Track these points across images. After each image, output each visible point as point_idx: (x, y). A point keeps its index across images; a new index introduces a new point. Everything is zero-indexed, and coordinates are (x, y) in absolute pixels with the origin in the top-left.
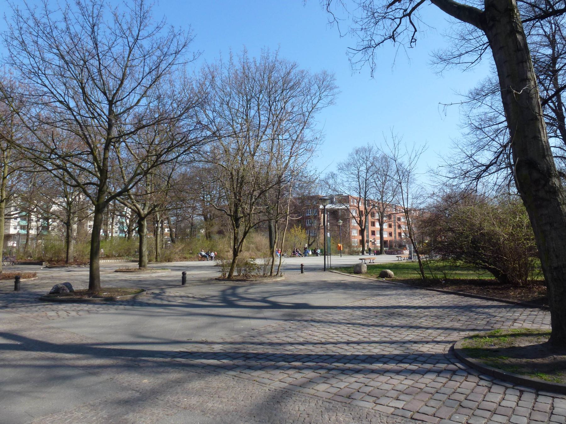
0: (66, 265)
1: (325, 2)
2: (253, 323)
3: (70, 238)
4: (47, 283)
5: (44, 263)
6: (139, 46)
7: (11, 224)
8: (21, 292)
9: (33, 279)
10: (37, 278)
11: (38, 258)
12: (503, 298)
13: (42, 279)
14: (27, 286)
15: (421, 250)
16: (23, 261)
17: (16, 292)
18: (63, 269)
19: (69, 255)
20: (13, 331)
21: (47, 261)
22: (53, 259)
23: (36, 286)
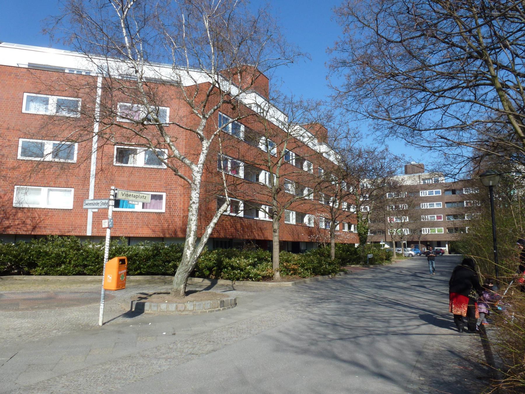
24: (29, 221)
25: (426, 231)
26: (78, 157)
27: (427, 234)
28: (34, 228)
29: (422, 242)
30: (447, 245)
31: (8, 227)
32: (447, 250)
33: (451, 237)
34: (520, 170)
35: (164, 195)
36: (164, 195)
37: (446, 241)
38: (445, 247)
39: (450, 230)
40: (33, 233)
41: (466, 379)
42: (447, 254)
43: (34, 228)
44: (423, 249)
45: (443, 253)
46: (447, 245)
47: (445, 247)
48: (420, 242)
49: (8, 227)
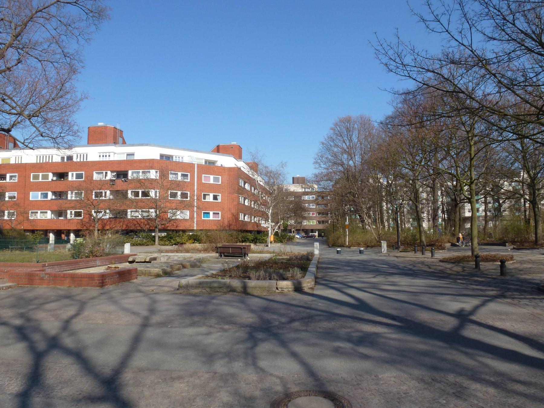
0: (536, 247)
1: (37, 401)
2: (454, 254)
3: (537, 217)
4: (530, 268)
5: (507, 244)
6: (537, 48)
7: (466, 208)
8: (508, 278)
9: (511, 262)
10: (515, 261)
11: (500, 239)
12: (384, 226)
13: (521, 262)
14: (511, 271)
15: (451, 217)
16: (486, 242)
17: (503, 277)
18: (535, 251)
19: (538, 236)
20: (535, 335)
21: (510, 242)
22: (516, 240)
23: (520, 271)
24: (175, 224)
25: (305, 223)
26: (29, 195)
27: (306, 225)
28: (177, 227)
29: (303, 230)
30: (317, 232)
31: (168, 227)
32: (317, 235)
33: (321, 227)
34: (387, 213)
35: (220, 212)
36: (220, 212)
37: (316, 229)
38: (316, 233)
39: (319, 222)
40: (176, 229)
41: (381, 207)
42: (317, 237)
43: (177, 227)
44: (303, 234)
45: (315, 237)
46: (317, 232)
47: (316, 233)
48: (271, 238)
49: (168, 227)
